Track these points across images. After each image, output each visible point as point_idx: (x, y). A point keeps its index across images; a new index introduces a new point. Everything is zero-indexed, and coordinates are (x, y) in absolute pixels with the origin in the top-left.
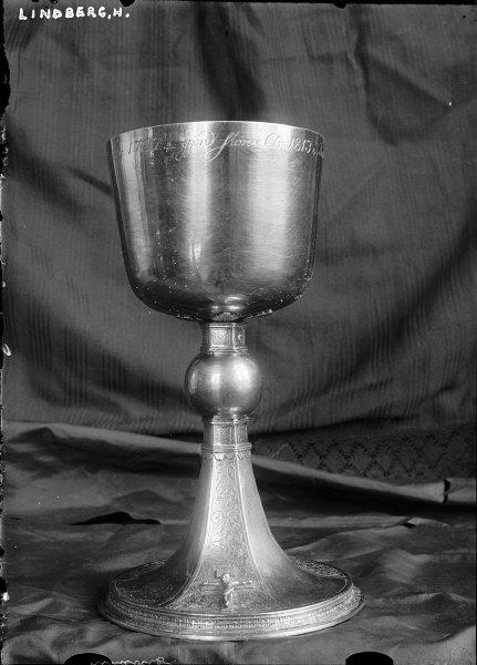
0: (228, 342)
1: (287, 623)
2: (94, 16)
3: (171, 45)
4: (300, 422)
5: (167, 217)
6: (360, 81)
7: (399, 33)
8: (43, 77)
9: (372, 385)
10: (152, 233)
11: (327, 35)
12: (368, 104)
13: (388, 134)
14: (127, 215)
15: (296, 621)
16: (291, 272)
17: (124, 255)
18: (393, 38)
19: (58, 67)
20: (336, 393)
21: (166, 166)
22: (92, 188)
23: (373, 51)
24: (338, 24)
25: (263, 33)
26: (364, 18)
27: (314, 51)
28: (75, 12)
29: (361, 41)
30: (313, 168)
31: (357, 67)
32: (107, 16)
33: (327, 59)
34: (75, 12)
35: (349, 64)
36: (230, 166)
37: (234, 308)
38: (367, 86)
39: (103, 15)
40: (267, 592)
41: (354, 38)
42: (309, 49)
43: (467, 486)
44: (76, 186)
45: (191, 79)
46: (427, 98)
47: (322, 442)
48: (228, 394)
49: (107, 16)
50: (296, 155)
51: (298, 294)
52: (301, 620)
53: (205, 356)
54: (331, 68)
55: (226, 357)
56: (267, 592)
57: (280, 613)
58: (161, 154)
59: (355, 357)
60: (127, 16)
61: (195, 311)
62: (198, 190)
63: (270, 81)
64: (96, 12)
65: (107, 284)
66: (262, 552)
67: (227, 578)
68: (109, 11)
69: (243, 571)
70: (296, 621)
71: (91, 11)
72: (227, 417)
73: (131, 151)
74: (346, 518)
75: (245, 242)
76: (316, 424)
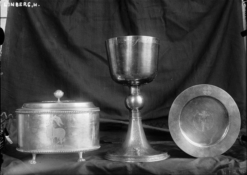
0: (136, 91)
1: (153, 158)
2: (26, 6)
3: (112, 14)
4: (148, 117)
5: (121, 59)
6: (164, 25)
7: (174, 12)
8: (77, 23)
9: (168, 107)
10: (117, 63)
11: (155, 12)
12: (166, 31)
13: (171, 39)
14: (110, 59)
15: (155, 158)
16: (152, 73)
17: (109, 68)
18: (173, 13)
19: (81, 20)
20: (158, 109)
21: (120, 47)
22: (90, 54)
23: (168, 17)
24: (158, 9)
25: (138, 12)
26: (165, 8)
27: (152, 16)
28: (19, 5)
29: (164, 14)
30: (157, 47)
31: (163, 21)
32: (31, 6)
33: (155, 19)
34: (19, 5)
35: (161, 20)
36: (137, 47)
37: (137, 82)
38: (166, 26)
39: (29, 6)
40: (146, 152)
41: (162, 13)
42: (150, 16)
43: (171, 172)
44: (86, 53)
45: (118, 26)
46: (182, 29)
47: (154, 123)
48: (136, 103)
49: (31, 6)
50: (153, 44)
51: (154, 79)
52: (156, 158)
53: (130, 95)
54: (156, 21)
55: (135, 95)
56: (146, 152)
57: (151, 156)
58: (119, 44)
59: (163, 100)
60: (39, 6)
61: (127, 84)
62: (129, 53)
63: (140, 25)
64: (27, 4)
65: (94, 80)
66: (143, 143)
67: (137, 149)
68: (31, 4)
69: (141, 148)
70: (155, 158)
71: (25, 4)
72: (135, 110)
73: (112, 43)
74: (162, 142)
75: (141, 65)
76: (153, 118)
